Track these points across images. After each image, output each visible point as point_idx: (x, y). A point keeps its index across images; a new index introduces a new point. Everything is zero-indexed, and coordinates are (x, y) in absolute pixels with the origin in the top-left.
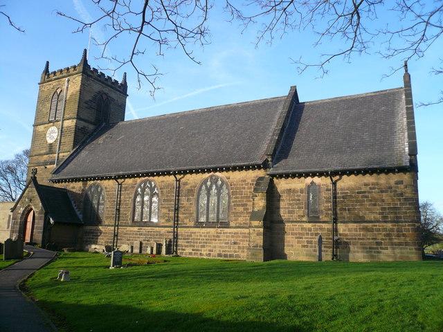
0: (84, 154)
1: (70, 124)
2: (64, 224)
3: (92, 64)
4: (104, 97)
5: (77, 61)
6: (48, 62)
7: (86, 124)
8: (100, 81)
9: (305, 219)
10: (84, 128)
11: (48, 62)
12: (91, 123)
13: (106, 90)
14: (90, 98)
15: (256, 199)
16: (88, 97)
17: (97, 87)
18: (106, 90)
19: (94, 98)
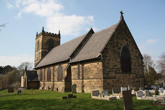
0: (44, 59)
1: (41, 51)
2: (98, 101)
3: (46, 31)
4: (51, 40)
5: (41, 31)
6: (43, 27)
7: (45, 50)
8: (49, 36)
9: (77, 78)
10: (45, 51)
11: (43, 27)
12: (47, 49)
13: (52, 38)
14: (46, 42)
15: (65, 72)
16: (45, 41)
17: (48, 38)
18: (52, 38)
19: (48, 41)
